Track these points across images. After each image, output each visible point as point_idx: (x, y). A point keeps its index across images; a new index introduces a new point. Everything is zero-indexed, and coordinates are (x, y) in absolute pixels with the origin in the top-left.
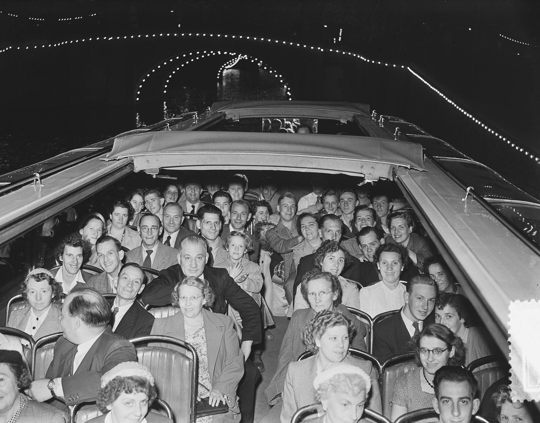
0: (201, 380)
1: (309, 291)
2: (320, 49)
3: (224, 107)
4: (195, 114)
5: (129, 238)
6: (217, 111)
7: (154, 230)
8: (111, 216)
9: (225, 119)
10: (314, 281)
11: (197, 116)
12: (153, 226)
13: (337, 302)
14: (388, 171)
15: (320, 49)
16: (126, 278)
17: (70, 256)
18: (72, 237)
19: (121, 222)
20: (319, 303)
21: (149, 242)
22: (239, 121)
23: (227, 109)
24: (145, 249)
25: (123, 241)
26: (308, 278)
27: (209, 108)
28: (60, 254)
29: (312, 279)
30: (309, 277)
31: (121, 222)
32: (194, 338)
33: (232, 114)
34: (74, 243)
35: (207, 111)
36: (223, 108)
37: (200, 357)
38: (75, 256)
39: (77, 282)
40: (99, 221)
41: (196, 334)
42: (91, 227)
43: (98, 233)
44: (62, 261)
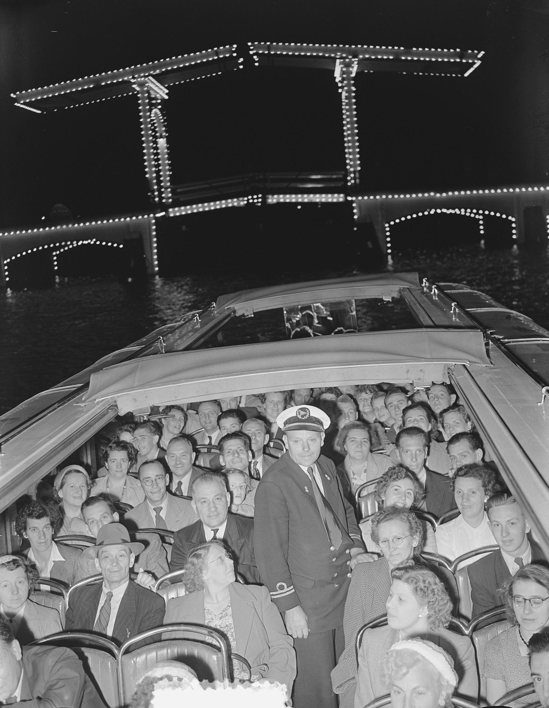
0: (238, 673)
1: (380, 536)
2: (490, 212)
3: (233, 300)
4: (196, 316)
5: (131, 490)
6: (224, 308)
7: (159, 480)
8: (106, 464)
9: (235, 316)
10: (385, 523)
11: (198, 318)
12: (157, 476)
13: (418, 548)
14: (442, 372)
15: (490, 212)
16: (107, 557)
17: (34, 530)
18: (33, 507)
19: (119, 470)
20: (394, 552)
21: (156, 497)
22: (253, 316)
23: (234, 303)
24: (152, 507)
25: (125, 494)
26: (378, 519)
27: (213, 304)
28: (22, 531)
29: (382, 522)
30: (379, 519)
31: (119, 470)
32: (221, 618)
33: (243, 308)
34: (36, 514)
35: (212, 308)
36: (231, 302)
37: (233, 643)
38: (41, 529)
39: (53, 561)
40: (80, 474)
41: (224, 613)
42: (72, 485)
43: (81, 490)
44: (27, 538)
